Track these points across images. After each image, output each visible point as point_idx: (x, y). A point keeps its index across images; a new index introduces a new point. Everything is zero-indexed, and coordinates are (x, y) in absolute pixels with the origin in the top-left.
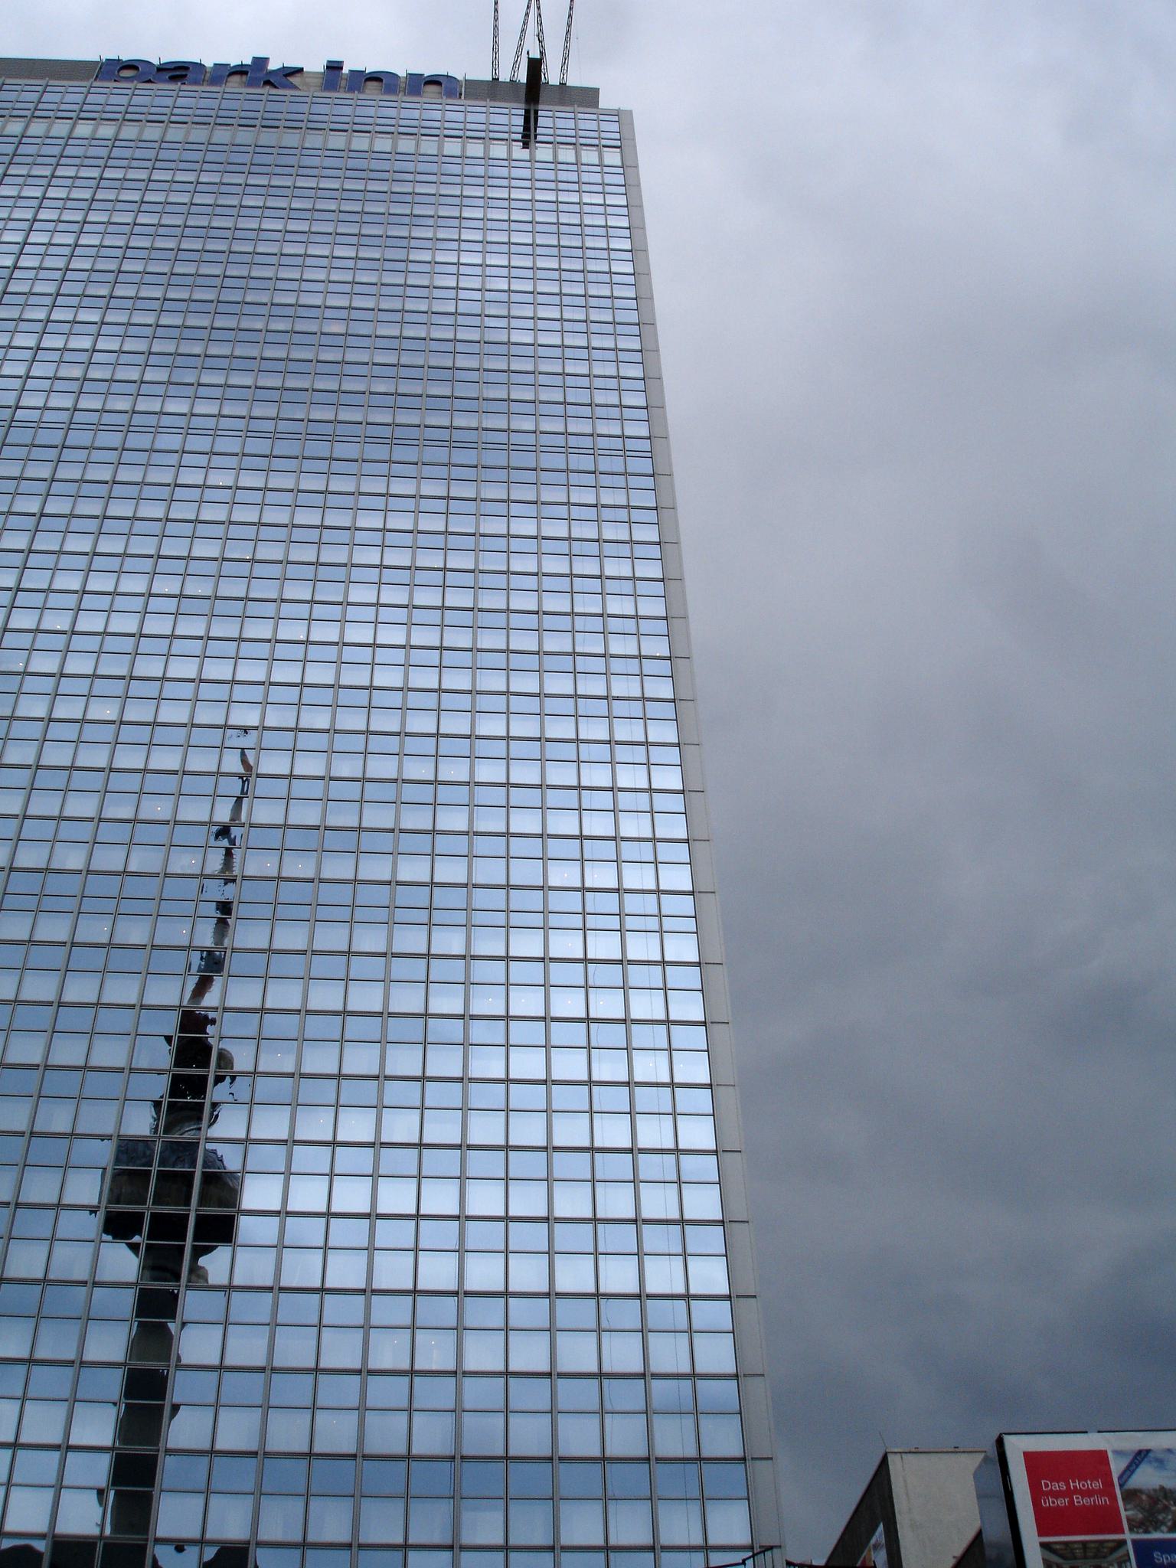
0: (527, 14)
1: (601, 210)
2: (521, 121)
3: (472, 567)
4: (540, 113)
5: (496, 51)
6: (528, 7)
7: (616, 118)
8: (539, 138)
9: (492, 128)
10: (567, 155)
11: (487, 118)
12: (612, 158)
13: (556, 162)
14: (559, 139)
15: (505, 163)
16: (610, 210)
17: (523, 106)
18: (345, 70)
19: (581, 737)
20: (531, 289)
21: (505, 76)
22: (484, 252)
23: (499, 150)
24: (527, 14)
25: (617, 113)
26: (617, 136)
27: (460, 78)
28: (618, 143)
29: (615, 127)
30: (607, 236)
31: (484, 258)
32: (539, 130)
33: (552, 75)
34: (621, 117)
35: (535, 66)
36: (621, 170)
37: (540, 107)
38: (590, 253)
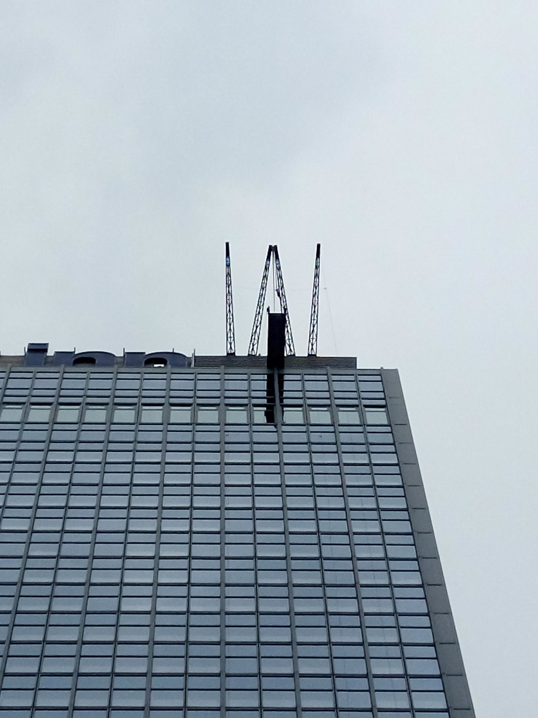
0: (265, 277)
1: (367, 469)
2: (264, 385)
3: (218, 555)
4: (286, 377)
5: (229, 314)
6: (266, 269)
7: (378, 378)
8: (286, 402)
9: (227, 394)
10: (320, 417)
11: (222, 385)
12: (376, 417)
13: (307, 424)
14: (310, 402)
15: (246, 428)
16: (376, 469)
17: (265, 371)
18: (50, 353)
19: (336, 672)
20: (290, 671)
21: (242, 351)
22: (223, 690)
23: (237, 416)
24: (265, 277)
25: (380, 373)
26: (382, 395)
27: (189, 355)
28: (383, 402)
29: (379, 387)
30: (392, 598)
31: (222, 634)
32: (285, 394)
33: (298, 345)
34: (388, 379)
35: (278, 324)
36: (388, 429)
37: (286, 371)
38: (374, 651)
